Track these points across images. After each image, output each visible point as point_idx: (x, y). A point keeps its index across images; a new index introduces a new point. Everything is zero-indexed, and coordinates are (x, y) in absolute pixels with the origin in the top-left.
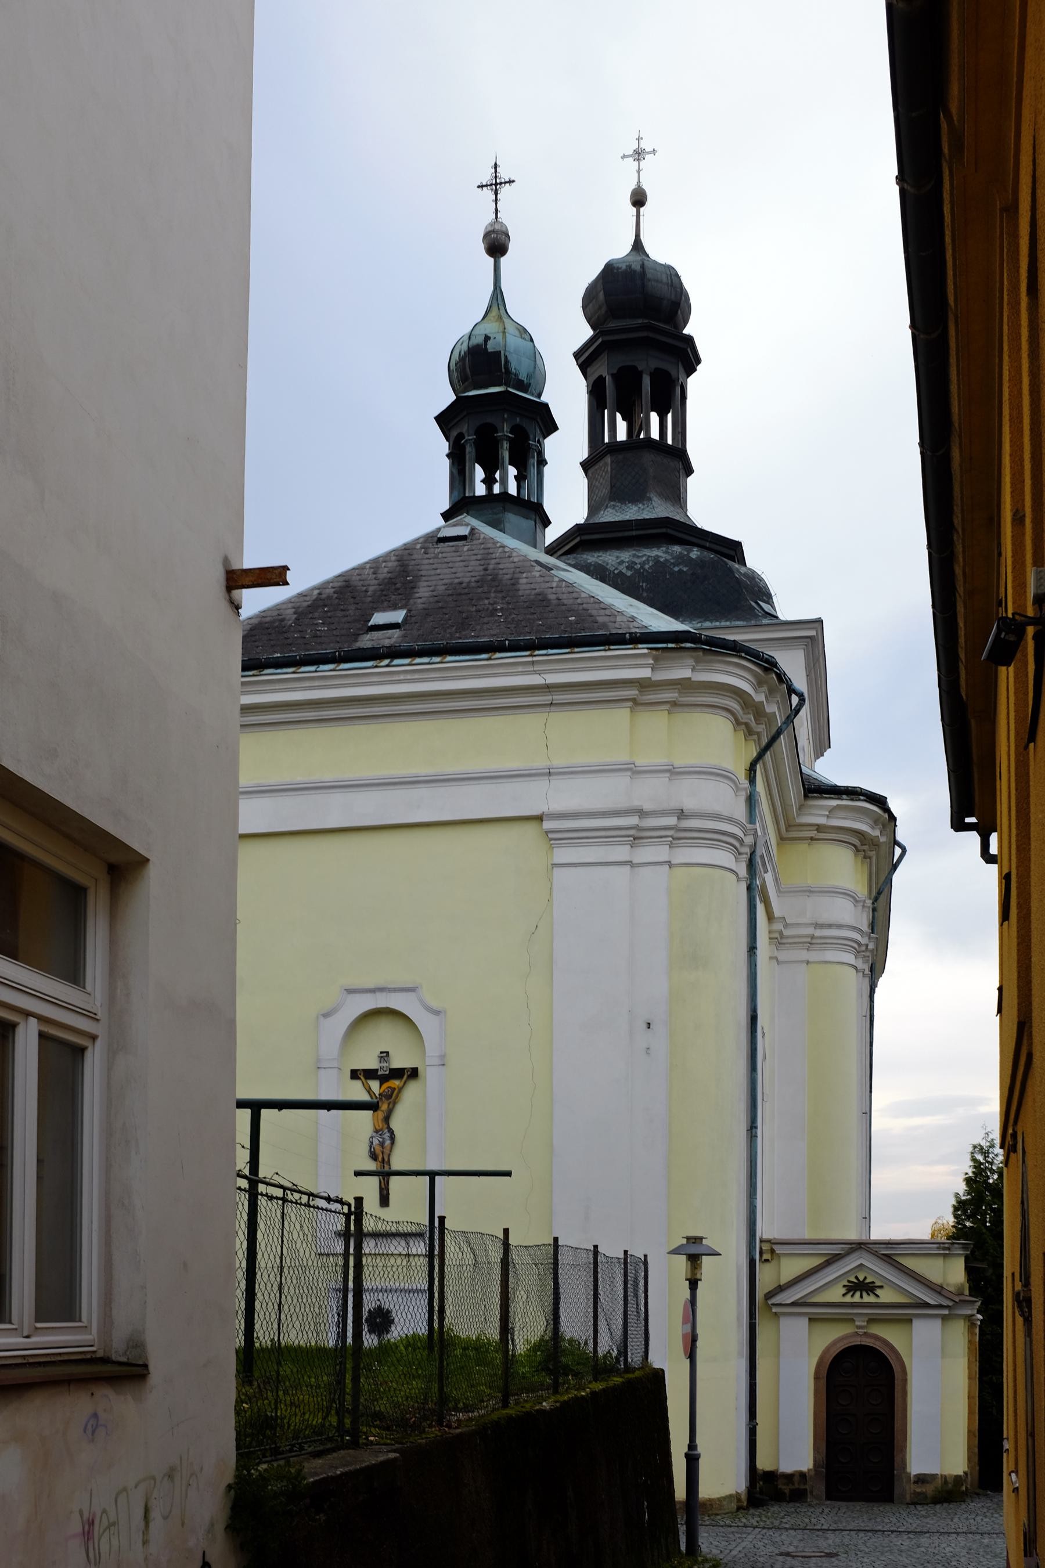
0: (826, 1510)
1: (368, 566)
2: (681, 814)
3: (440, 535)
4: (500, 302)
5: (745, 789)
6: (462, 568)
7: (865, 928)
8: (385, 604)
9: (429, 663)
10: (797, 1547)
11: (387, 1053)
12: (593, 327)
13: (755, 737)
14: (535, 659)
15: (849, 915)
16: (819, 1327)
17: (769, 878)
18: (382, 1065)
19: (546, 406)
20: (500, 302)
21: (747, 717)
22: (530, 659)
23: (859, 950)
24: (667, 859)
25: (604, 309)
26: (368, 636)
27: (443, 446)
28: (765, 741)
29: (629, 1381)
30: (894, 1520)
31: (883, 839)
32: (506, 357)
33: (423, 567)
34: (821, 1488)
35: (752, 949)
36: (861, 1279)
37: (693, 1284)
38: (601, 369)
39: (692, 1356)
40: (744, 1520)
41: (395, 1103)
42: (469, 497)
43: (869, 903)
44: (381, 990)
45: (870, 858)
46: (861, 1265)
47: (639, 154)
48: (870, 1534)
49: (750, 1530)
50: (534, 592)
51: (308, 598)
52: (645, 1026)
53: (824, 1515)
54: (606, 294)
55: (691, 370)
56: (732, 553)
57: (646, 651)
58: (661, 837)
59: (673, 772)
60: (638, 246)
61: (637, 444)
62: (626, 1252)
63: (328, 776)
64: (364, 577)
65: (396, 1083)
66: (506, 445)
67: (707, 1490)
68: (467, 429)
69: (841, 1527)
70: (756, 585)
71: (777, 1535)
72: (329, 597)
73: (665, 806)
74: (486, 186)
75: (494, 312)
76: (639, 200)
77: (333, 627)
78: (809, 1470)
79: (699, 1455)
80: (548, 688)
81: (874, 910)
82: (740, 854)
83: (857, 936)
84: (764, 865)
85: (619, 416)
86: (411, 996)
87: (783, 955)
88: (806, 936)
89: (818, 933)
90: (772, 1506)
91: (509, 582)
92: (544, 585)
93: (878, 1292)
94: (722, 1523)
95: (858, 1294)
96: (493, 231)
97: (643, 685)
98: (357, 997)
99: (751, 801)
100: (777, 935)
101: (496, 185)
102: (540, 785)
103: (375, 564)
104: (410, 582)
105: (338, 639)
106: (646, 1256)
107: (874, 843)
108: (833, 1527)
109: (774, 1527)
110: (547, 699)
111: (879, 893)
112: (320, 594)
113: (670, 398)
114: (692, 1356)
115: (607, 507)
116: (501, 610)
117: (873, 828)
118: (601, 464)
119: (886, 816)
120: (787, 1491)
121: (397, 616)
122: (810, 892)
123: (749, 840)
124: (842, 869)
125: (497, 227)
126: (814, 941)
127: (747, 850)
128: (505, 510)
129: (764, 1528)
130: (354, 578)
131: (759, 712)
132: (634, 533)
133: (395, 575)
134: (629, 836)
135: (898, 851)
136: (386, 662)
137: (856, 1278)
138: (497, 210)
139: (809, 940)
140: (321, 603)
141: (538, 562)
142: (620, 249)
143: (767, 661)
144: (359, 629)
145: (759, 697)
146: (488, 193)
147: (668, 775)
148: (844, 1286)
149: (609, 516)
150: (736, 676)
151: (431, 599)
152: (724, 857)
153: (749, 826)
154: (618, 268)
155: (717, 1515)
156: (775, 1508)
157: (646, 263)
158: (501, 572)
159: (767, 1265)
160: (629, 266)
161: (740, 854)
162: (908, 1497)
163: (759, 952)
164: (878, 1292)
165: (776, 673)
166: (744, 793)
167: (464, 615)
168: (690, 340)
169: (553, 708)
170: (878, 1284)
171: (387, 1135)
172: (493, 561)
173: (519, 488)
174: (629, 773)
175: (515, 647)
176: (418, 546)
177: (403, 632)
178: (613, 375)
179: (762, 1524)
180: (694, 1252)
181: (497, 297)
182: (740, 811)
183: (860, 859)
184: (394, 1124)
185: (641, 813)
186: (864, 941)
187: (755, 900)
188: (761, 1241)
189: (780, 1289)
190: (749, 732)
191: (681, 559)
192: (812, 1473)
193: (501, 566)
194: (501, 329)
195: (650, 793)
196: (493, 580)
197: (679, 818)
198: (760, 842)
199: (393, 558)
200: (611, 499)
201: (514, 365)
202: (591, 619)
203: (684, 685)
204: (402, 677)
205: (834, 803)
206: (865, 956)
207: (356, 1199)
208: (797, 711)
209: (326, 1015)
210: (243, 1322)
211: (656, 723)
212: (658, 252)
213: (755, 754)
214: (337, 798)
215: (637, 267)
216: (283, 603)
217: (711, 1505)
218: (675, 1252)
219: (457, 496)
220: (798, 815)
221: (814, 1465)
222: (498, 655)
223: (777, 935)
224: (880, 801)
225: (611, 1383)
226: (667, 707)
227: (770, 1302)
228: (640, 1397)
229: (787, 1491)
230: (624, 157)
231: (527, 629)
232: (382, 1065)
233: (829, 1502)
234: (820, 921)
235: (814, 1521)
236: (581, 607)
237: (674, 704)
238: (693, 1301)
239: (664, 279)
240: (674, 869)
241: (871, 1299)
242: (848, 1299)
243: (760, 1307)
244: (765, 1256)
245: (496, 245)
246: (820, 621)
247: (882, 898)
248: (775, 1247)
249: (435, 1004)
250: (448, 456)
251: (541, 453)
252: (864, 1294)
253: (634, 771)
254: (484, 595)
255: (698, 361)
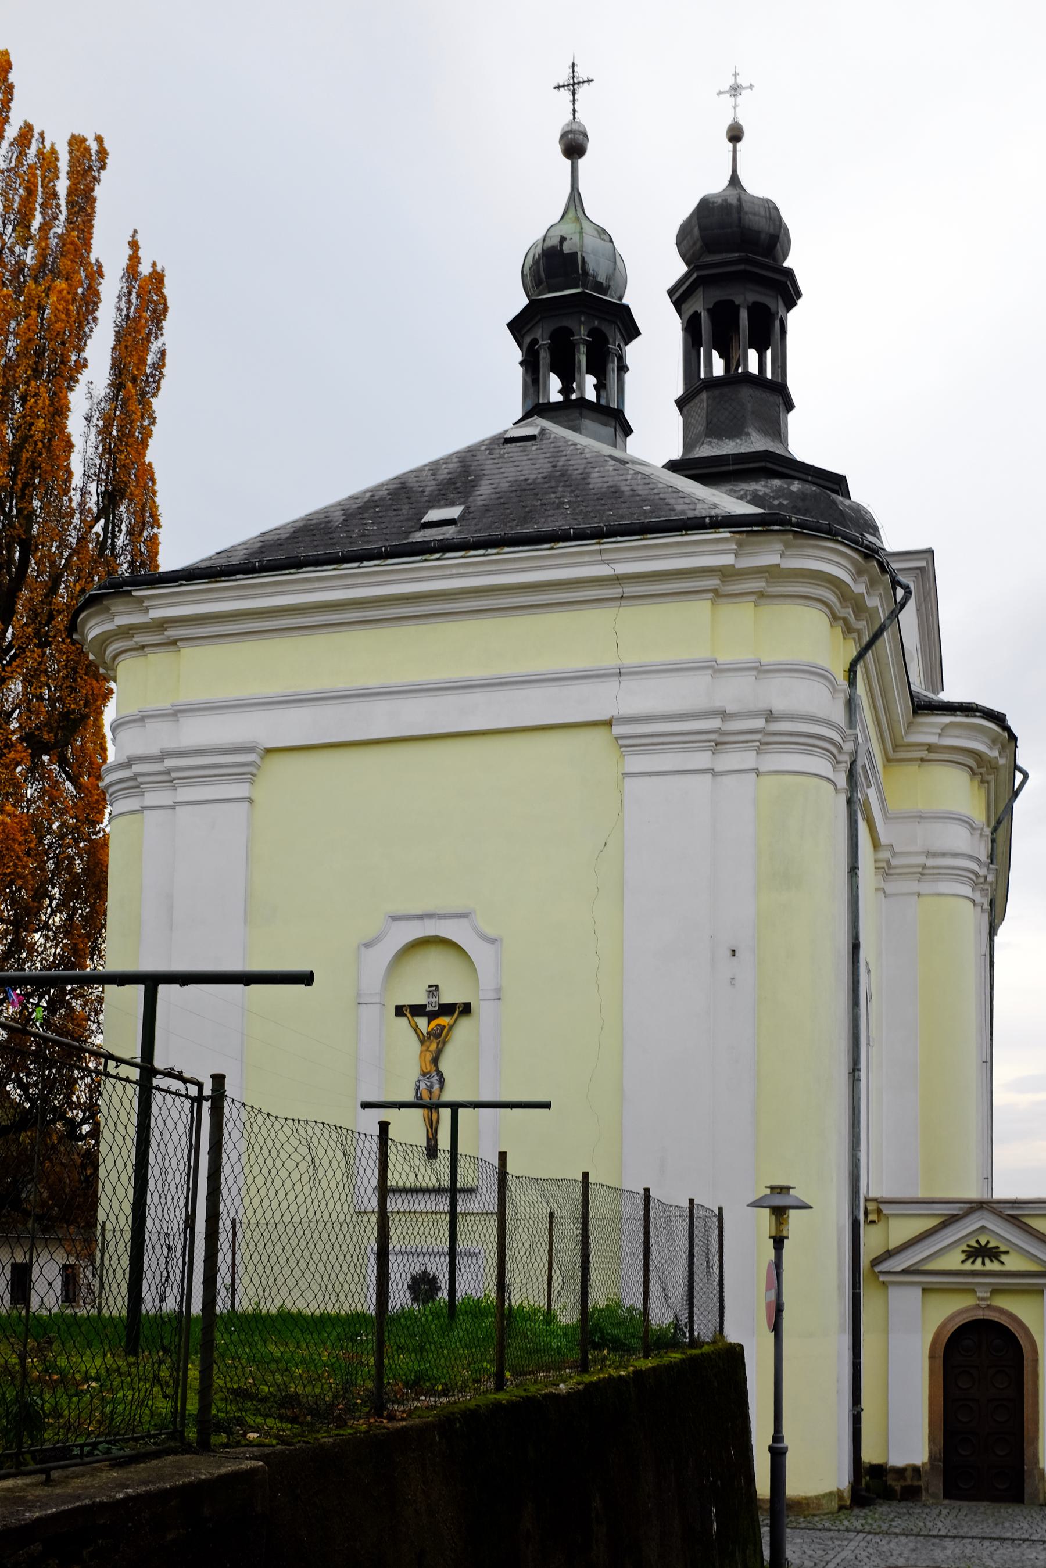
0: (944, 1512)
1: (427, 468)
2: (770, 716)
3: (507, 436)
4: (577, 203)
5: (844, 691)
6: (529, 466)
7: (984, 857)
8: (442, 502)
9: (484, 555)
10: (908, 1559)
11: (437, 986)
12: (687, 264)
13: (855, 635)
14: (603, 547)
15: (965, 843)
16: (935, 1299)
17: (872, 793)
18: (431, 1000)
19: (627, 308)
20: (577, 203)
21: (843, 609)
22: (597, 547)
23: (976, 881)
24: (754, 767)
25: (699, 244)
26: (421, 533)
27: (516, 354)
28: (866, 638)
29: (693, 1359)
30: (1026, 1526)
31: (1002, 761)
32: (583, 258)
33: (486, 467)
34: (937, 1485)
35: (853, 869)
36: (983, 1243)
37: (779, 1242)
38: (697, 304)
39: (777, 1328)
40: (846, 1523)
41: (444, 1043)
42: (543, 404)
43: (987, 831)
44: (430, 916)
45: (988, 782)
46: (983, 1228)
47: (735, 90)
48: (997, 1543)
49: (852, 1535)
50: (606, 485)
51: (359, 501)
52: (729, 953)
53: (942, 1517)
54: (701, 229)
55: (791, 304)
56: (836, 487)
57: (728, 535)
58: (747, 742)
59: (760, 670)
60: (734, 181)
61: (736, 379)
62: (691, 1201)
63: (373, 682)
64: (421, 479)
65: (444, 1021)
66: (583, 349)
67: (795, 1487)
68: (542, 336)
69: (962, 1533)
70: (862, 517)
71: (884, 1542)
72: (382, 499)
73: (752, 707)
74: (563, 86)
75: (571, 214)
76: (735, 135)
77: (383, 526)
78: (924, 1464)
79: (787, 1448)
80: (618, 579)
81: (993, 841)
82: (838, 762)
83: (974, 866)
84: (867, 777)
85: (715, 354)
86: (464, 922)
87: (891, 887)
88: (918, 866)
89: (930, 862)
90: (881, 1505)
91: (579, 477)
92: (617, 478)
93: (1003, 1258)
94: (820, 1526)
95: (979, 1261)
96: (570, 132)
97: (725, 573)
98: (403, 924)
99: (851, 705)
100: (884, 864)
101: (573, 86)
102: (611, 686)
103: (435, 467)
104: (472, 481)
105: (387, 537)
106: (720, 1209)
107: (992, 767)
108: (953, 1532)
109: (882, 1532)
110: (617, 591)
111: (999, 822)
112: (372, 496)
113: (768, 333)
114: (777, 1328)
115: (703, 443)
116: (569, 502)
117: (991, 748)
118: (696, 401)
119: (1006, 734)
120: (898, 1488)
121: (454, 512)
122: (921, 817)
123: (848, 747)
124: (957, 792)
125: (575, 127)
126: (926, 871)
127: (846, 758)
128: (581, 416)
129: (869, 1533)
130: (410, 480)
131: (859, 607)
132: (731, 468)
133: (458, 477)
134: (710, 741)
135: (1019, 777)
136: (438, 555)
137: (978, 1242)
138: (574, 110)
139: (920, 870)
140: (372, 504)
141: (610, 457)
142: (716, 185)
143: (867, 547)
144: (412, 527)
145: (859, 588)
146: (566, 94)
147: (755, 673)
148: (963, 1251)
149: (705, 451)
150: (830, 561)
151: (493, 496)
152: (820, 765)
153: (848, 732)
154: (714, 203)
155: (814, 1515)
156: (884, 1509)
157: (743, 196)
158: (571, 468)
159: (873, 1227)
160: (725, 200)
161: (838, 762)
162: (1041, 1497)
163: (860, 873)
164: (1003, 1258)
165: (878, 560)
166: (842, 695)
167: (527, 509)
168: (789, 273)
169: (624, 602)
170: (1003, 1249)
171: (435, 1079)
172: (563, 458)
173: (598, 396)
174: (710, 672)
175: (581, 536)
176: (483, 448)
177: (459, 528)
178: (709, 310)
179: (867, 1528)
180: (780, 1206)
181: (575, 199)
182: (839, 715)
183: (976, 783)
184: (443, 1066)
185: (724, 715)
186: (983, 872)
187: (856, 815)
188: (866, 1200)
189: (889, 1254)
190: (848, 630)
191: (780, 493)
192: (928, 1467)
193: (571, 463)
194: (578, 230)
195: (734, 693)
196: (562, 475)
197: (767, 721)
198: (862, 751)
199: (456, 460)
200: (707, 436)
201: (591, 266)
202: (668, 507)
203: (772, 573)
204: (454, 571)
205: (947, 719)
206: (983, 890)
207: (213, 1077)
208: (902, 605)
209: (368, 945)
210: (145, 1266)
211: (741, 615)
212: (755, 186)
213: (855, 654)
214: (382, 707)
215: (734, 201)
216: (332, 506)
217: (808, 1504)
218: (757, 1204)
219: (530, 405)
220: (906, 734)
221: (930, 1457)
222: (561, 544)
223: (884, 864)
224: (998, 718)
225: (666, 1360)
226: (753, 598)
227: (877, 1269)
228: (713, 1379)
229: (898, 1488)
230: (720, 93)
231: (596, 520)
232: (431, 1000)
233: (946, 1502)
234: (932, 849)
235: (929, 1525)
236: (657, 497)
237: (761, 595)
238: (778, 1264)
239: (762, 213)
240: (762, 778)
241: (995, 1266)
242: (968, 1266)
243: (862, 1274)
244: (871, 1217)
245: (574, 147)
246: (930, 552)
247: (1002, 828)
248: (882, 1206)
249: (490, 932)
250: (521, 363)
251: (621, 358)
252: (987, 1261)
253: (715, 668)
254: (550, 490)
255: (799, 295)
